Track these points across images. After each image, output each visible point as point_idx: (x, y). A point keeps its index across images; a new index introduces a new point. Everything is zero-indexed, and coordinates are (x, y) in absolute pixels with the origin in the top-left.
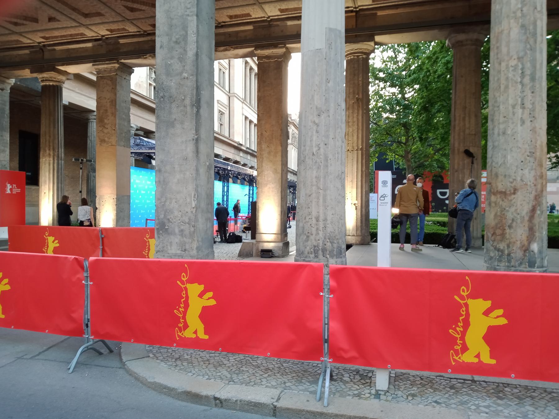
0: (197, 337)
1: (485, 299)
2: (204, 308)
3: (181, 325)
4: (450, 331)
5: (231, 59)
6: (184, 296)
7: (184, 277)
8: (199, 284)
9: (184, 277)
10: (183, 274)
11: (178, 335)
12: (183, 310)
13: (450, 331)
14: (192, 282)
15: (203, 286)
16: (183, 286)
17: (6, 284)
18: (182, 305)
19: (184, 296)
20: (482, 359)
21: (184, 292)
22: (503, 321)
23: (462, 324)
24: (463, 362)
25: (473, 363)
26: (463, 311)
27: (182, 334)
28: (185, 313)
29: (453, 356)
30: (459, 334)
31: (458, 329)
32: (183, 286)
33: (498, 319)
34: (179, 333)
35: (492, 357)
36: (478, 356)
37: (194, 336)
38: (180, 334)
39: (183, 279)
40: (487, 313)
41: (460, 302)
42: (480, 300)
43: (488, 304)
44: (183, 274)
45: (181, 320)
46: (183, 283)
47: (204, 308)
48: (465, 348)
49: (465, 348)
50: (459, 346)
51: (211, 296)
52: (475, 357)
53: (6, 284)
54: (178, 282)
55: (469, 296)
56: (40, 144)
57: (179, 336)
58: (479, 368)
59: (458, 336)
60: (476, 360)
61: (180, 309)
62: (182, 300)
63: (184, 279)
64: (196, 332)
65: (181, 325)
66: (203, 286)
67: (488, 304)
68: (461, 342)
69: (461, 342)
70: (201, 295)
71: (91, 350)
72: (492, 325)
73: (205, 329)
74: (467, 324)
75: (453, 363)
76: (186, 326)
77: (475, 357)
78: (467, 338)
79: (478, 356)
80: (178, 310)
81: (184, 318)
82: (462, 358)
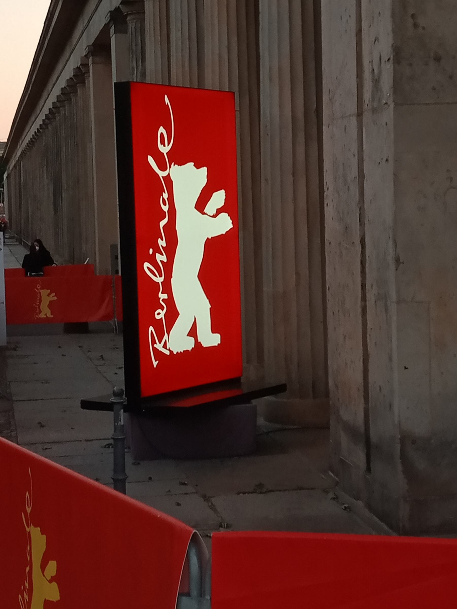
1: (48, 289)
6: (165, 208)
8: (198, 166)
15: (204, 170)
17: (219, 211)
20: (48, 316)
21: (165, 196)
22: (55, 298)
32: (162, 174)
33: (53, 297)
36: (46, 315)
38: (159, 346)
40: (49, 295)
45: (163, 296)
49: (40, 312)
51: (221, 203)
54: (151, 160)
55: (40, 289)
57: (157, 352)
58: (47, 320)
59: (159, 280)
60: (45, 316)
71: (45, 574)
74: (40, 301)
79: (46, 315)
80: (36, 304)
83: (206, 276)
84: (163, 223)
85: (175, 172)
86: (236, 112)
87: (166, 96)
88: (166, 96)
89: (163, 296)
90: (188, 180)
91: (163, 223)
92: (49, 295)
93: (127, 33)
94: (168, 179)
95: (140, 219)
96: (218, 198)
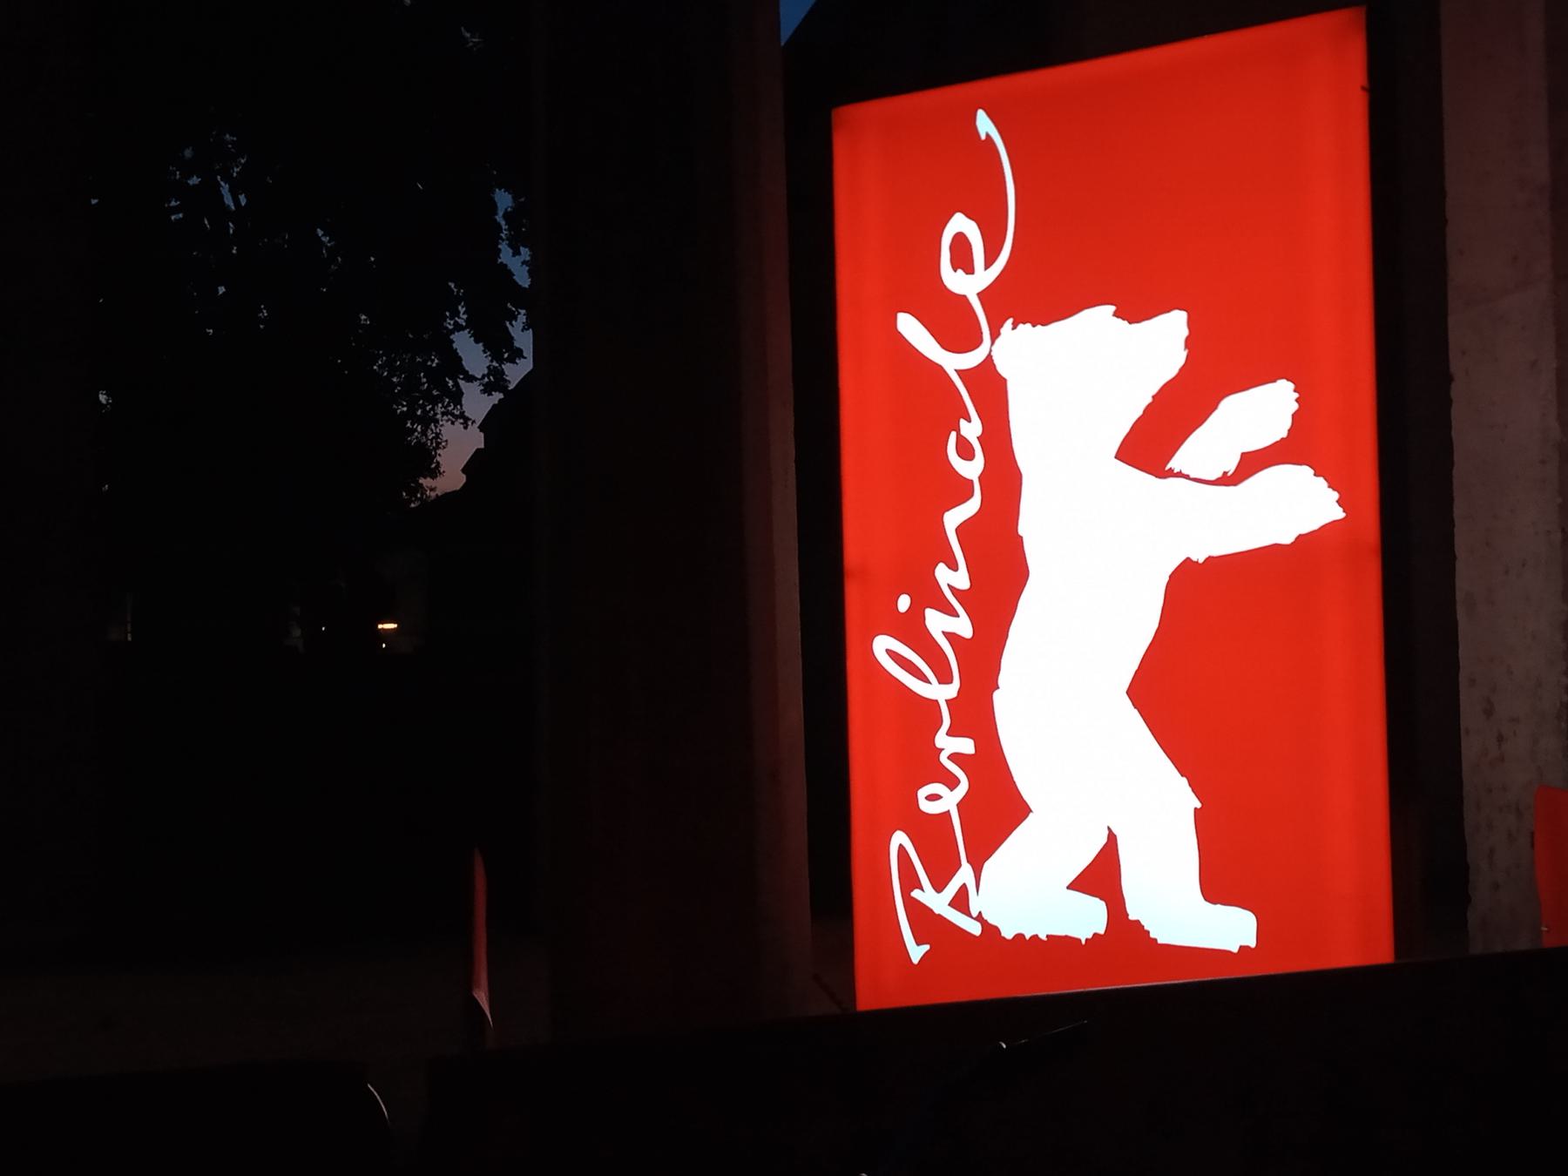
0: (1123, 929)
3: (942, 800)
4: (883, 645)
6: (971, 469)
7: (963, 260)
8: (1133, 312)
9: (963, 260)
10: (960, 223)
11: (918, 912)
12: (963, 626)
15: (1173, 327)
16: (953, 363)
17: (1251, 464)
18: (954, 578)
19: (971, 469)
21: (972, 429)
23: (961, 579)
24: (990, 930)
25: (1061, 945)
26: (966, 451)
27: (960, 901)
28: (981, 661)
29: (910, 881)
30: (945, 678)
31: (936, 622)
32: (953, 363)
34: (927, 896)
35: (1218, 885)
36: (1101, 877)
37: (1086, 919)
38: (937, 902)
39: (954, 280)
41: (938, 370)
44: (960, 223)
45: (950, 745)
46: (955, 326)
50: (952, 783)
52: (1077, 885)
57: (924, 920)
59: (942, 693)
61: (936, 622)
62: (953, 519)
63: (968, 285)
64: (1101, 877)
65: (942, 800)
66: (1173, 327)
67: (1163, 344)
68: (966, 746)
69: (966, 746)
70: (1151, 444)
72: (1200, 556)
75: (916, 952)
76: (997, 808)
77: (1077, 885)
78: (1011, 706)
81: (975, 713)
82: (975, 906)
83: (1160, 691)
84: (953, 519)
85: (1018, 351)
87: (450, 476)
89: (950, 745)
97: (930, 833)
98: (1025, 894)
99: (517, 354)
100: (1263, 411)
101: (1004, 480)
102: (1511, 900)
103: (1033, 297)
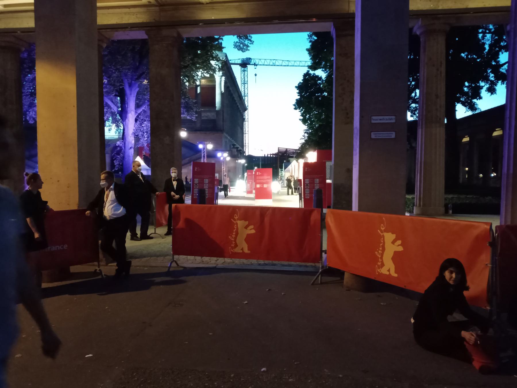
2: (395, 253)
4: (230, 237)
5: (33, 14)
8: (393, 233)
13: (230, 237)
14: (241, 220)
15: (395, 235)
16: (382, 234)
17: (399, 245)
18: (381, 249)
22: (253, 231)
25: (386, 274)
28: (382, 255)
32: (382, 234)
35: (396, 272)
36: (389, 271)
38: (379, 270)
42: (390, 234)
43: (247, 223)
45: (380, 260)
47: (395, 253)
48: (236, 246)
49: (236, 246)
53: (399, 245)
56: (236, 79)
57: (232, 252)
59: (380, 256)
63: (383, 229)
65: (379, 264)
66: (395, 235)
67: (247, 223)
70: (393, 242)
73: (395, 268)
76: (383, 265)
78: (384, 258)
81: (382, 258)
83: (393, 259)
84: (381, 245)
85: (386, 234)
86: (156, 232)
87: (114, 241)
88: (114, 241)
89: (380, 260)
90: (389, 237)
91: (381, 245)
92: (246, 227)
93: (414, 193)
94: (383, 235)
95: (377, 243)
96: (399, 242)
97: (378, 266)
98: (384, 271)
99: (330, 159)
100: (252, 227)
101: (384, 243)
102: (321, 209)
103: (386, 231)
